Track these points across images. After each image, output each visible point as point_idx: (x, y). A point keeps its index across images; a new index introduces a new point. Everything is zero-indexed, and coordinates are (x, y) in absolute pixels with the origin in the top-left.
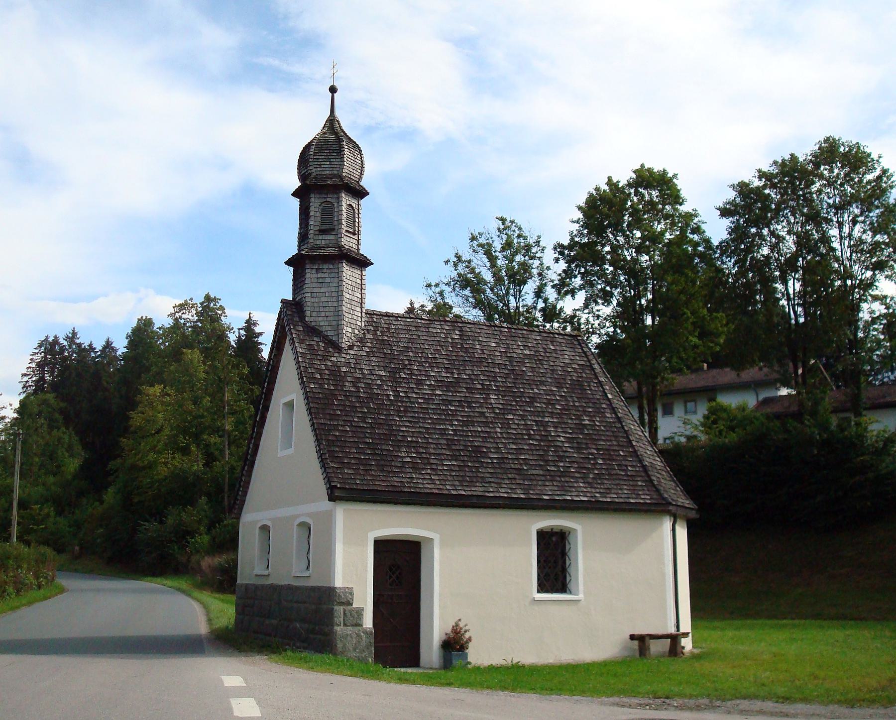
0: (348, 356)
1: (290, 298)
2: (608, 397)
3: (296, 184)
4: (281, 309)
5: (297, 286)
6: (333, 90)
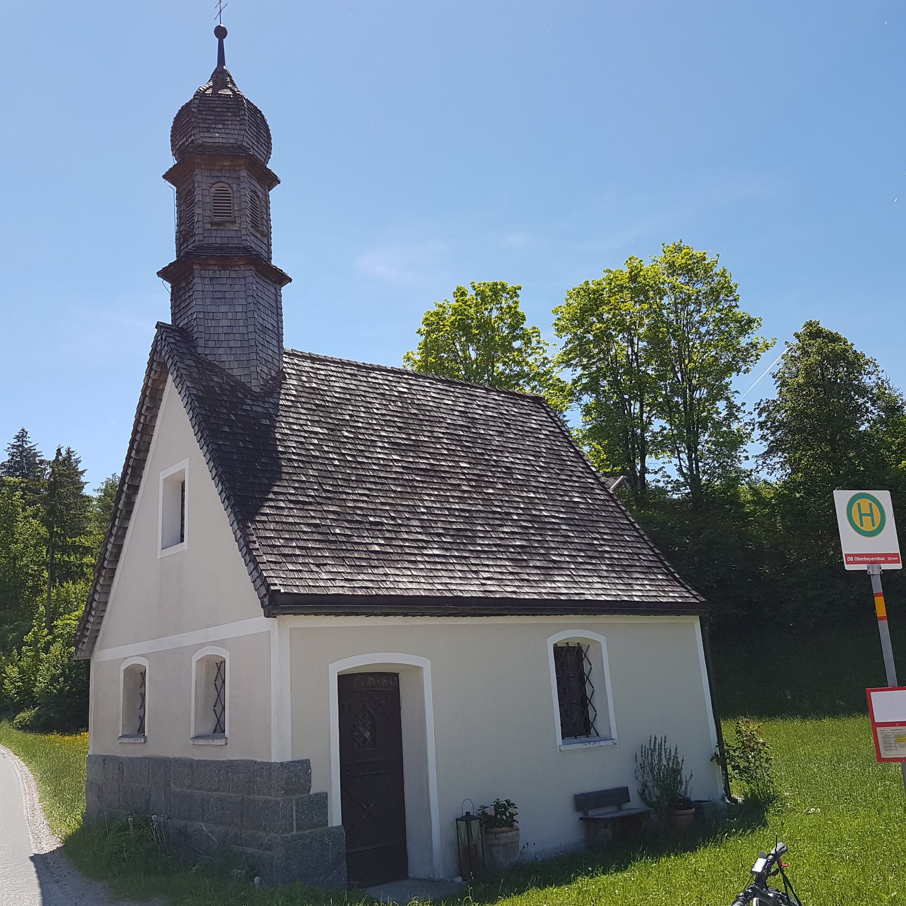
0: (267, 405)
1: (168, 321)
2: (591, 470)
3: (171, 161)
4: (156, 336)
5: (174, 318)
6: (221, 33)
